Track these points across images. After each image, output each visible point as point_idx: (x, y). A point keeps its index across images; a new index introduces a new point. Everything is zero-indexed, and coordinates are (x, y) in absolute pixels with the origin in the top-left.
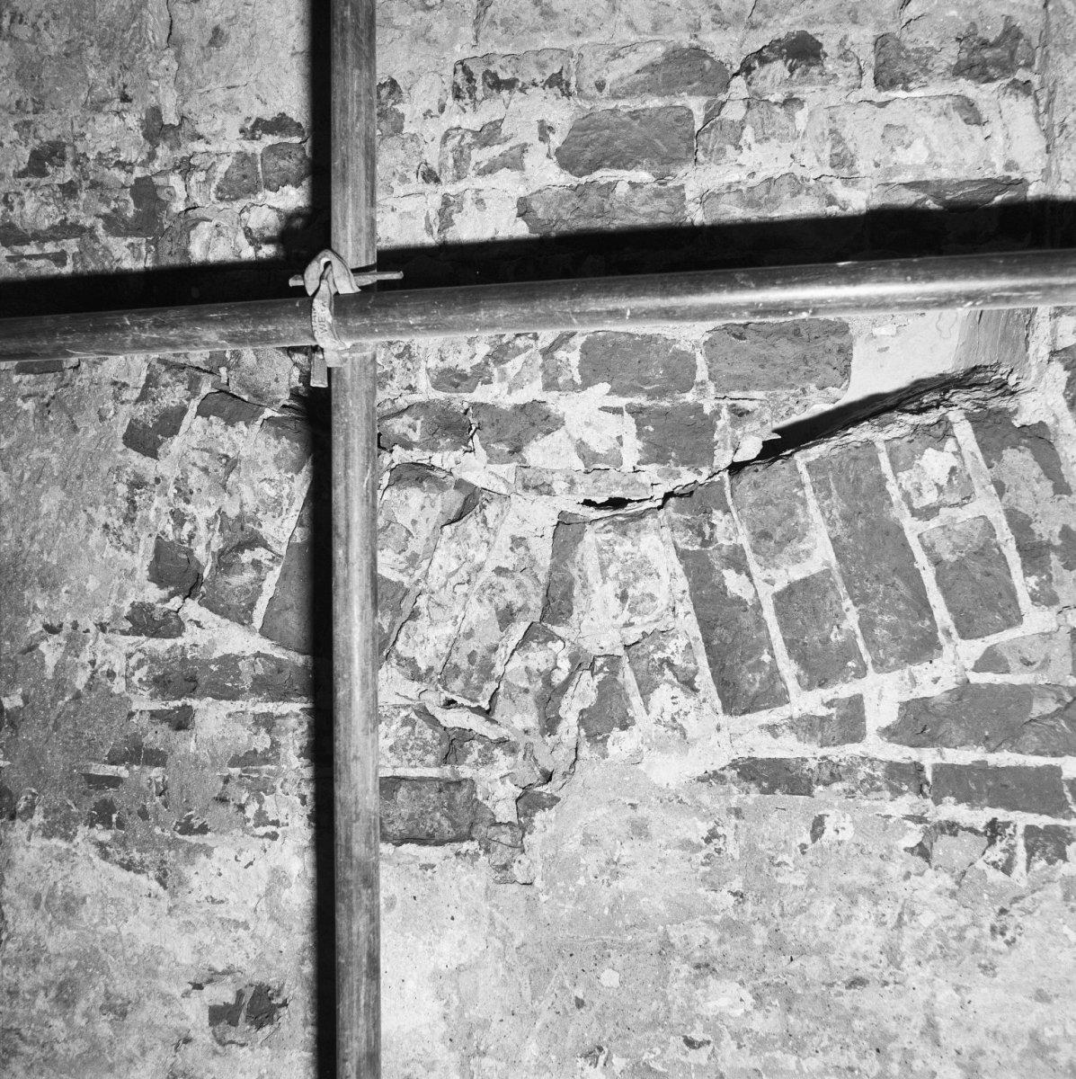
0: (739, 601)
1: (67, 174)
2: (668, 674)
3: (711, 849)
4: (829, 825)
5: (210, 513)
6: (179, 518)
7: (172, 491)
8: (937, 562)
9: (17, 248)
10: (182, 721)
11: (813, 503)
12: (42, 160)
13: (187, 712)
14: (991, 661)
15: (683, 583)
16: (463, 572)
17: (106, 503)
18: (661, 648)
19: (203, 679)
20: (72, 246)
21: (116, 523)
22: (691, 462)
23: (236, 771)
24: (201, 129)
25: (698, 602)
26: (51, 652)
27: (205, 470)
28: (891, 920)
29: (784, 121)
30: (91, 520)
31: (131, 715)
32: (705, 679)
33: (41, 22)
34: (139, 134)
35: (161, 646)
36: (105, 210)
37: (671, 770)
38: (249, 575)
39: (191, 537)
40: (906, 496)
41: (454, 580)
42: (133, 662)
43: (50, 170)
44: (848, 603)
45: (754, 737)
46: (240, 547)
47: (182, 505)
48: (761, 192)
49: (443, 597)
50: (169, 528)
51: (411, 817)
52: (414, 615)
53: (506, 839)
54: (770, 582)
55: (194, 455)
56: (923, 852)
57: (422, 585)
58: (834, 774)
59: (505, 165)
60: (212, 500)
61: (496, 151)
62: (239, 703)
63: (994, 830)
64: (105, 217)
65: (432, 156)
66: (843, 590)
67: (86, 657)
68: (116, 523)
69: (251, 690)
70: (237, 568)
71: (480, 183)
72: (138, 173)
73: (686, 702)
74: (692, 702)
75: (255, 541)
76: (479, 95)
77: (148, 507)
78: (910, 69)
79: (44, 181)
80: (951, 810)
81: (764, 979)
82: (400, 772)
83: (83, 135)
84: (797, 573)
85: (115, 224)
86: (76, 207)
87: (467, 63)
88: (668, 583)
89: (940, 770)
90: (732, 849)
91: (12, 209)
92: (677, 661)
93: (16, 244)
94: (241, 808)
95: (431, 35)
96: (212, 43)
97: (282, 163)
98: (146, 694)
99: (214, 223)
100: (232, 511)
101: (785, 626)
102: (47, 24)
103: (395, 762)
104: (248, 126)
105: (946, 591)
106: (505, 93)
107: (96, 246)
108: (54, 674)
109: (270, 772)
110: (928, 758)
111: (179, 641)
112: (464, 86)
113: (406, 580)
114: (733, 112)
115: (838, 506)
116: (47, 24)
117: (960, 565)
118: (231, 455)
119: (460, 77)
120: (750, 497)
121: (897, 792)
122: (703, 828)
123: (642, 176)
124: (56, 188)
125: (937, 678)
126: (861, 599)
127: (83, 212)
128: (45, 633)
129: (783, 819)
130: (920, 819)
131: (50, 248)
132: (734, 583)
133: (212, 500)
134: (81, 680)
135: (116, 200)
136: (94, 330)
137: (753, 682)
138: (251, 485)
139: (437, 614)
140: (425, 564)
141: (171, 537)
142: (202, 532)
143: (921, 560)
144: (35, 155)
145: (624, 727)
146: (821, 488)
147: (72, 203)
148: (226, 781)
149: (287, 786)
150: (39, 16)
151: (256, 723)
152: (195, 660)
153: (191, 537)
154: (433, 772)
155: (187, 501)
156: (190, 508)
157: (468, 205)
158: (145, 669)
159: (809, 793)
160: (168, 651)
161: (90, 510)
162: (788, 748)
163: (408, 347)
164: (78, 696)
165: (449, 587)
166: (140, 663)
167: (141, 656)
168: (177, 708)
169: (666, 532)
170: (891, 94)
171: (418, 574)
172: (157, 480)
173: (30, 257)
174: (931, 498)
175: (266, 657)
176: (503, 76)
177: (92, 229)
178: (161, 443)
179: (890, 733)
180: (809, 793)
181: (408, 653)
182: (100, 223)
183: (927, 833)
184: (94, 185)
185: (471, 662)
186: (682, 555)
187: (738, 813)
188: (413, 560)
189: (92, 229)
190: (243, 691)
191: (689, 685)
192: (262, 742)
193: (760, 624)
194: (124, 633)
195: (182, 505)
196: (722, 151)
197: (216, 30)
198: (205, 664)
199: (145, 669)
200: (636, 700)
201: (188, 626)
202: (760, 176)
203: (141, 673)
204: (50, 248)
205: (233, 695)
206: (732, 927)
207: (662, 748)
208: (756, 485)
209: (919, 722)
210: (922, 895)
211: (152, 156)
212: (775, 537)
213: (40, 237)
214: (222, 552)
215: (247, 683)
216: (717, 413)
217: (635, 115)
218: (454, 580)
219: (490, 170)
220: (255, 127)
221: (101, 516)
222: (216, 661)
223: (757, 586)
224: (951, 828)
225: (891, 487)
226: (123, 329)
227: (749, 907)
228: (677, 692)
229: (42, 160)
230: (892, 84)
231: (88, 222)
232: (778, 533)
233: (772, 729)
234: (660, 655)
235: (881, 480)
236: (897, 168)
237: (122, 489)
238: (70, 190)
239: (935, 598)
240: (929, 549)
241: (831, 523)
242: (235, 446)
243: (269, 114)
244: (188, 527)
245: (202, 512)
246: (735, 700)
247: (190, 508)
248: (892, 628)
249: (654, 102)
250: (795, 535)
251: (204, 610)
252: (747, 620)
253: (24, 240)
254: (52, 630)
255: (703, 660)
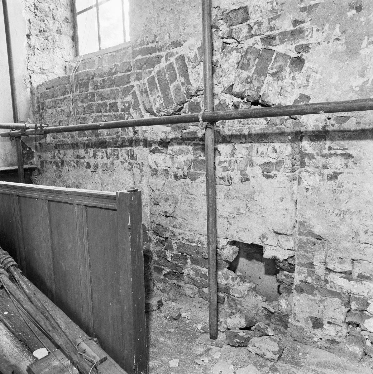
0: (182, 77)
1: (326, 172)
2: (192, 60)
3: (184, 26)
4: (168, 37)
5: (285, 81)
6: (294, 78)
7: (296, 85)
8: (157, 88)
9: (344, 152)
10: (295, 22)
11: (173, 96)
12: (334, 176)
13: (294, 26)
14: (150, 72)
15: (190, 78)
16: (227, 75)
17: (316, 80)
18: (193, 65)
19: (289, 36)
20: (326, 152)
21: (313, 75)
22: (193, 103)
23: (279, 13)
24: (287, 178)
25: (188, 76)
26: (337, 32)
27: (286, 91)
28: (159, 22)
29: (179, 165)
30: (321, 74)
31: (310, 20)
32: (186, 61)
33: (331, 213)
34: (303, 179)
35: (302, 42)
36: (314, 160)
37: (191, 41)
38: (275, 66)
39: (290, 74)
40: (161, 99)
41: (229, 72)
42: (310, 36)
43: (332, 173)
44: (168, 79)
45: (179, 51)
46: (276, 73)
47: (293, 82)
48: (181, 153)
49: (231, 68)
50: (297, 75)
51: (238, 15)
52: (238, 63)
53: (219, 16)
54: (178, 81)
55: (289, 95)
56: (156, 36)
57: (236, 70)
58: (168, 48)
59: (222, 162)
60: (285, 84)
61: (223, 165)
62: (280, 32)
63: (148, 44)
64: (314, 158)
65: (236, 166)
66: (169, 81)
67: (325, 34)
68: (313, 75)
69: (276, 36)
70: (277, 67)
71: (227, 159)
72: (303, 169)
73: (189, 55)
74: (188, 55)
75: (273, 75)
76: (227, 177)
77: (303, 80)
78: (163, 172)
79: (334, 170)
80: (153, 45)
81: (175, 4)
82: (241, 25)
83: (319, 181)
84: (174, 83)
85: (311, 157)
86: (322, 162)
87: (229, 184)
88: (192, 78)
89: (155, 52)
90: (181, 28)
91: (345, 163)
92: (191, 63)
93: (345, 154)
94: (277, 4)
95: (235, 191)
96: (283, 198)
97: (268, 168)
98: (305, 27)
99: (285, 155)
100: (280, 82)
101: (175, 73)
102: (329, 212)
103: (241, 27)
104: (275, 177)
105: (156, 83)
106: (221, 176)
107: (317, 151)
108: (336, 26)
109: (270, 16)
110: (157, 54)
111: (296, 45)
112: (230, 180)
113: (240, 70)
114: (186, 168)
115: (169, 96)
116: (329, 212)
117: (154, 88)
118: (279, 96)
119: (230, 181)
120: (181, 97)
121: (160, 46)
122: (186, 31)
123: (200, 158)
124: (329, 168)
125: (157, 68)
126: (166, 80)
127: (321, 161)
128: (340, 38)
129: (175, 36)
130: (157, 42)
131: (333, 152)
132: (183, 80)
133: (285, 84)
134: (327, 26)
135: (310, 163)
136: (245, 114)
137: (180, 62)
138: (275, 89)
139: (232, 64)
140: (236, 75)
141: (296, 73)
142: (287, 75)
143: (159, 89)
144: (337, 178)
145: (199, 47)
146: (172, 99)
147: (324, 163)
148: (281, 10)
149: (265, 13)
150: (331, 215)
151: (274, 28)
152: (291, 40)
153: (290, 74)
154: (234, 27)
155: (291, 83)
156: (291, 81)
157: (228, 154)
158: (306, 35)
159: (172, 42)
160: (299, 41)
161: (322, 77)
162: (174, 50)
163: (240, 124)
164: (328, 21)
165: (230, 71)
166: (308, 36)
167: (307, 38)
168: (297, 26)
169: (193, 88)
170: (165, 168)
171: (238, 73)
172: (300, 88)
173: (340, 149)
174: (158, 99)
175: (273, 46)
176: (222, 180)
177: (318, 155)
178: (299, 98)
179: (162, 57)
180: (172, 42)
181: (238, 54)
182: (315, 157)
183: (155, 40)
184: (318, 167)
185: (226, 55)
186: (190, 84)
187: (181, 35)
188: (239, 75)
189: (318, 155)
190: (278, 35)
191: (189, 59)
192: (273, 23)
193: (179, 73)
194: (312, 44)
195: (293, 82)
196: (187, 161)
197: (282, 201)
198: (289, 40)
199: (306, 35)
200: (198, 54)
201: (294, 49)
202: (182, 156)
203: (307, 33)
204: (333, 152)
205: (281, 33)
206: (180, 12)
207: (192, 45)
208: (181, 99)
209: (159, 59)
210: (155, 29)
211: (300, 173)
212: (178, 89)
213: (336, 155)
214: (282, 71)
215: (277, 38)
216: (188, 112)
217: (201, 170)
218: (229, 72)
219: (225, 161)
220: (274, 177)
221: (318, 76)
222: (286, 41)
223: (181, 79)
224: (153, 42)
225: (163, 100)
226: (239, 114)
227: (178, 17)
228: (190, 57)
229: (334, 176)
230: (166, 170)
231: (319, 157)
232: (177, 90)
233: (177, 53)
234: (193, 64)
235: (164, 102)
236: (164, 156)
237: (311, 84)
238: (325, 167)
239: (157, 82)
240: (158, 90)
241: (170, 93)
242: (278, 98)
243: (270, 179)
244: (291, 76)
245: (288, 80)
246: (182, 58)
247: (291, 81)
248: (162, 76)
249: (198, 172)
250: (175, 90)
251: (289, 54)
252: (181, 73)
253: (342, 155)
254: (338, 39)
255: (187, 64)
